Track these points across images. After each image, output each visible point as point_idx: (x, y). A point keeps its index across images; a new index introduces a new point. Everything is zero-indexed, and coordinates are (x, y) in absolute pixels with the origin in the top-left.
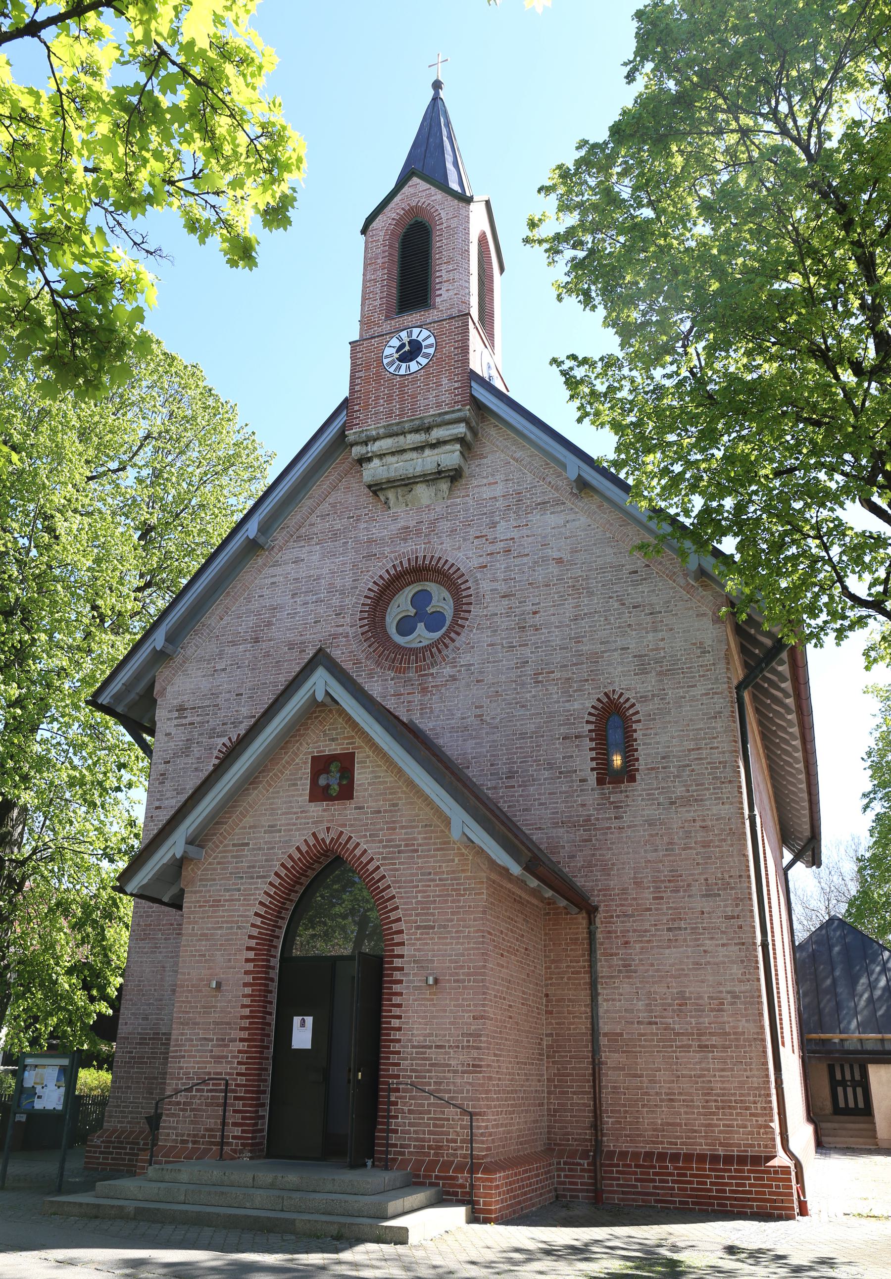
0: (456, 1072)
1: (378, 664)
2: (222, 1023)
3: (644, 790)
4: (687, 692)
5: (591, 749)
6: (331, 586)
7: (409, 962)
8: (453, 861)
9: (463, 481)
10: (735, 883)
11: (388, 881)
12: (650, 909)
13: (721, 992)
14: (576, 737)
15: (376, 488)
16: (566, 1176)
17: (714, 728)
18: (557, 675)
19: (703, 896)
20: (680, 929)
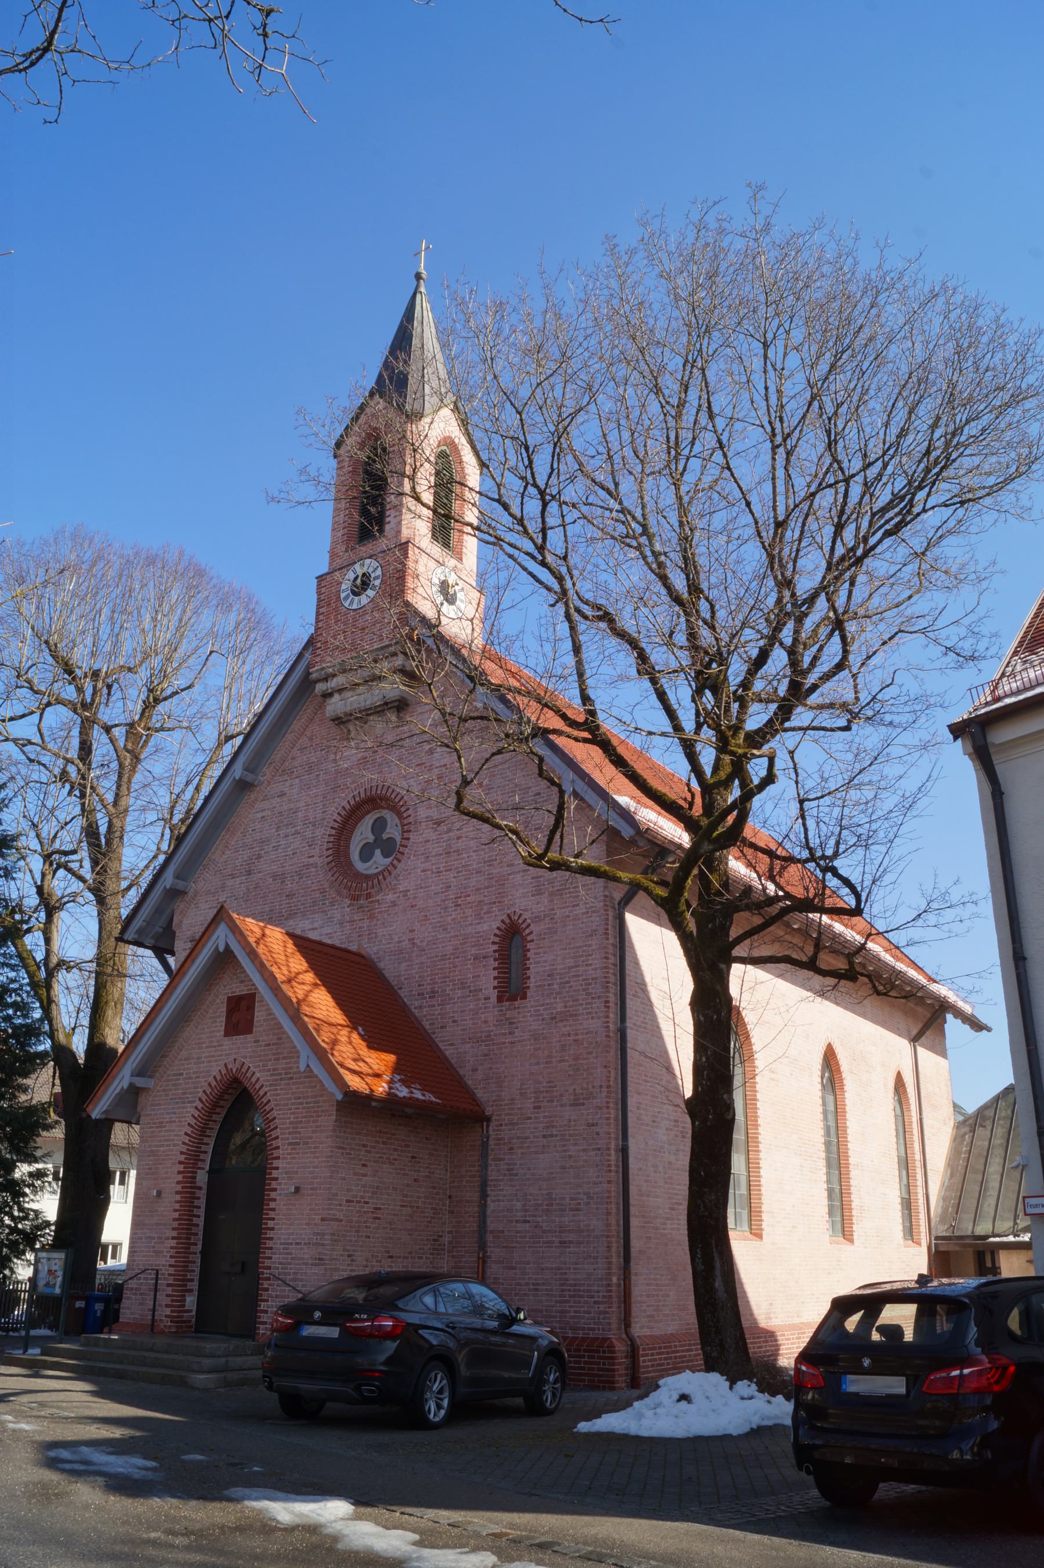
0: (307, 1264)
1: (339, 893)
3: (532, 1006)
4: (571, 911)
5: (494, 969)
8: (315, 1086)
11: (272, 1104)
13: (579, 1193)
14: (484, 957)
15: (339, 721)
17: (590, 946)
19: (572, 1105)
20: (552, 1136)
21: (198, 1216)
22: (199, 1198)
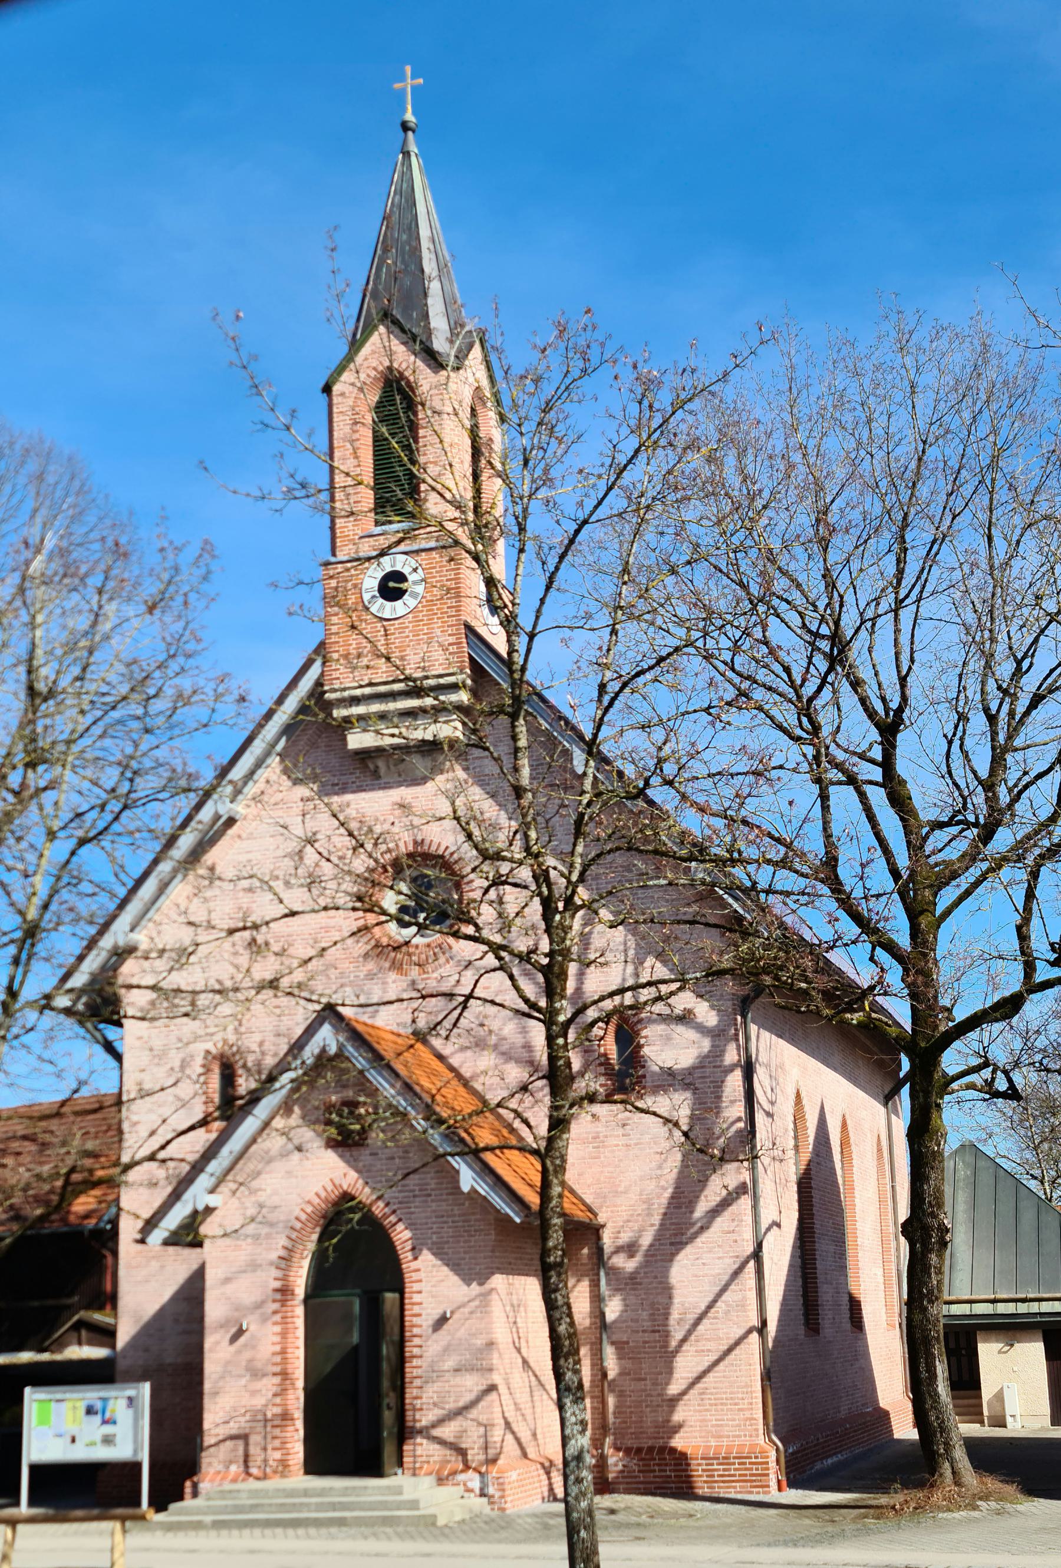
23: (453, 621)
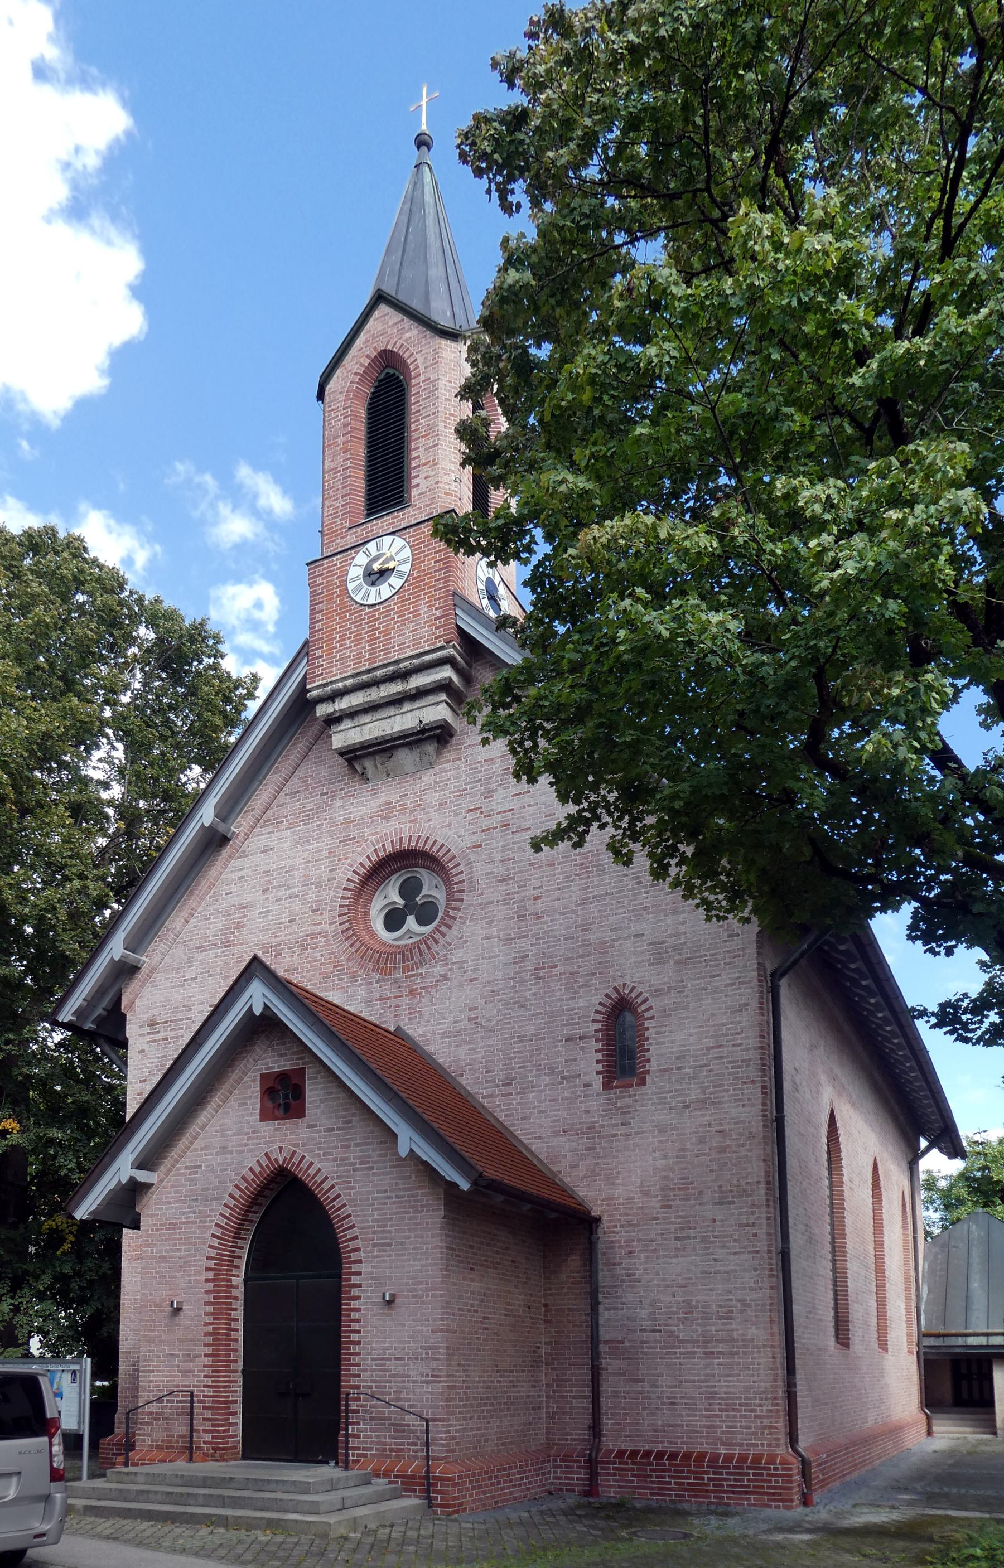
2: (186, 1340)
6: (306, 879)
7: (367, 1279)
9: (454, 741)
10: (753, 1190)
12: (657, 1218)
14: (581, 1038)
16: (562, 1472)
17: (739, 1022)
18: (560, 969)
19: (715, 1204)
20: (689, 1237)
21: (237, 1330)
22: (235, 1310)
23: (441, 593)
